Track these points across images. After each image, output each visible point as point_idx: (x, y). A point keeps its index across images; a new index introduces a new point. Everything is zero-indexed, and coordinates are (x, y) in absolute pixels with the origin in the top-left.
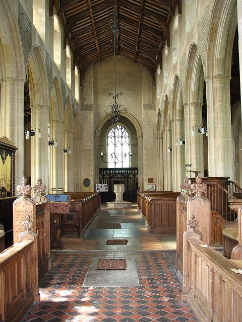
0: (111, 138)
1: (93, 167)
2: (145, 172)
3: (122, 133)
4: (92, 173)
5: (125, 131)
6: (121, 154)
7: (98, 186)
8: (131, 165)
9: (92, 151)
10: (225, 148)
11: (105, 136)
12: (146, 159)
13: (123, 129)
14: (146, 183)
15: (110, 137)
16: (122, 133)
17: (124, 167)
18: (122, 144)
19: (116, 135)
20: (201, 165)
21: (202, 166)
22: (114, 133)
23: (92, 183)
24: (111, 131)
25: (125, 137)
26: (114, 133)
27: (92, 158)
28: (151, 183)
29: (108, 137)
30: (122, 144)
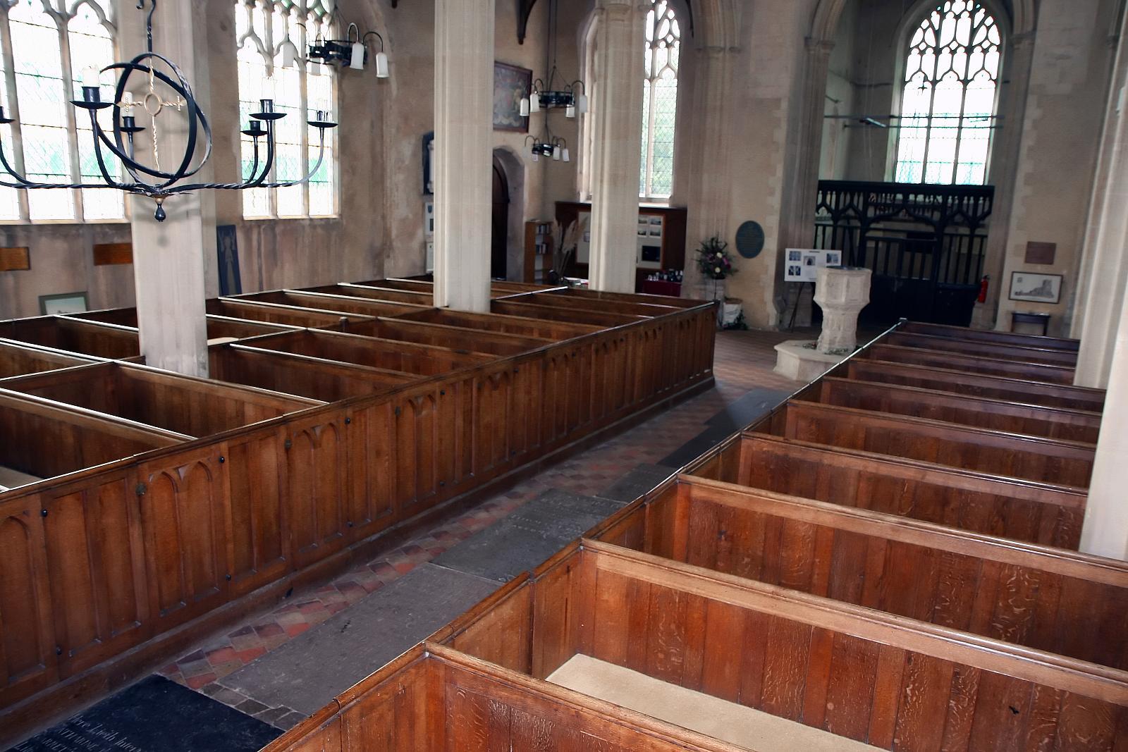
0: (922, 53)
1: (780, 172)
2: (1018, 210)
3: (974, 32)
4: (776, 201)
5: (990, 21)
6: (956, 122)
7: (794, 257)
8: (989, 181)
9: (784, 105)
10: (986, 247)
11: (892, 46)
12: (1030, 149)
13: (980, 15)
14: (1014, 261)
15: (915, 51)
16: (974, 32)
17: (929, 181)
18: (965, 82)
19: (945, 39)
20: (330, 205)
21: (17, 207)
22: (937, 34)
23: (771, 243)
24: (925, 24)
25: (985, 51)
26: (937, 34)
27: (781, 135)
28: (1040, 268)
29: (908, 51)
30: (965, 82)
